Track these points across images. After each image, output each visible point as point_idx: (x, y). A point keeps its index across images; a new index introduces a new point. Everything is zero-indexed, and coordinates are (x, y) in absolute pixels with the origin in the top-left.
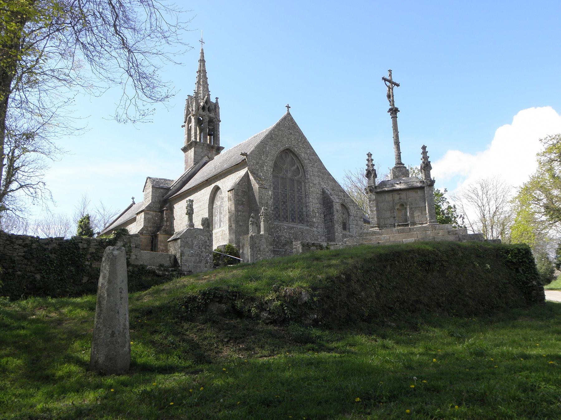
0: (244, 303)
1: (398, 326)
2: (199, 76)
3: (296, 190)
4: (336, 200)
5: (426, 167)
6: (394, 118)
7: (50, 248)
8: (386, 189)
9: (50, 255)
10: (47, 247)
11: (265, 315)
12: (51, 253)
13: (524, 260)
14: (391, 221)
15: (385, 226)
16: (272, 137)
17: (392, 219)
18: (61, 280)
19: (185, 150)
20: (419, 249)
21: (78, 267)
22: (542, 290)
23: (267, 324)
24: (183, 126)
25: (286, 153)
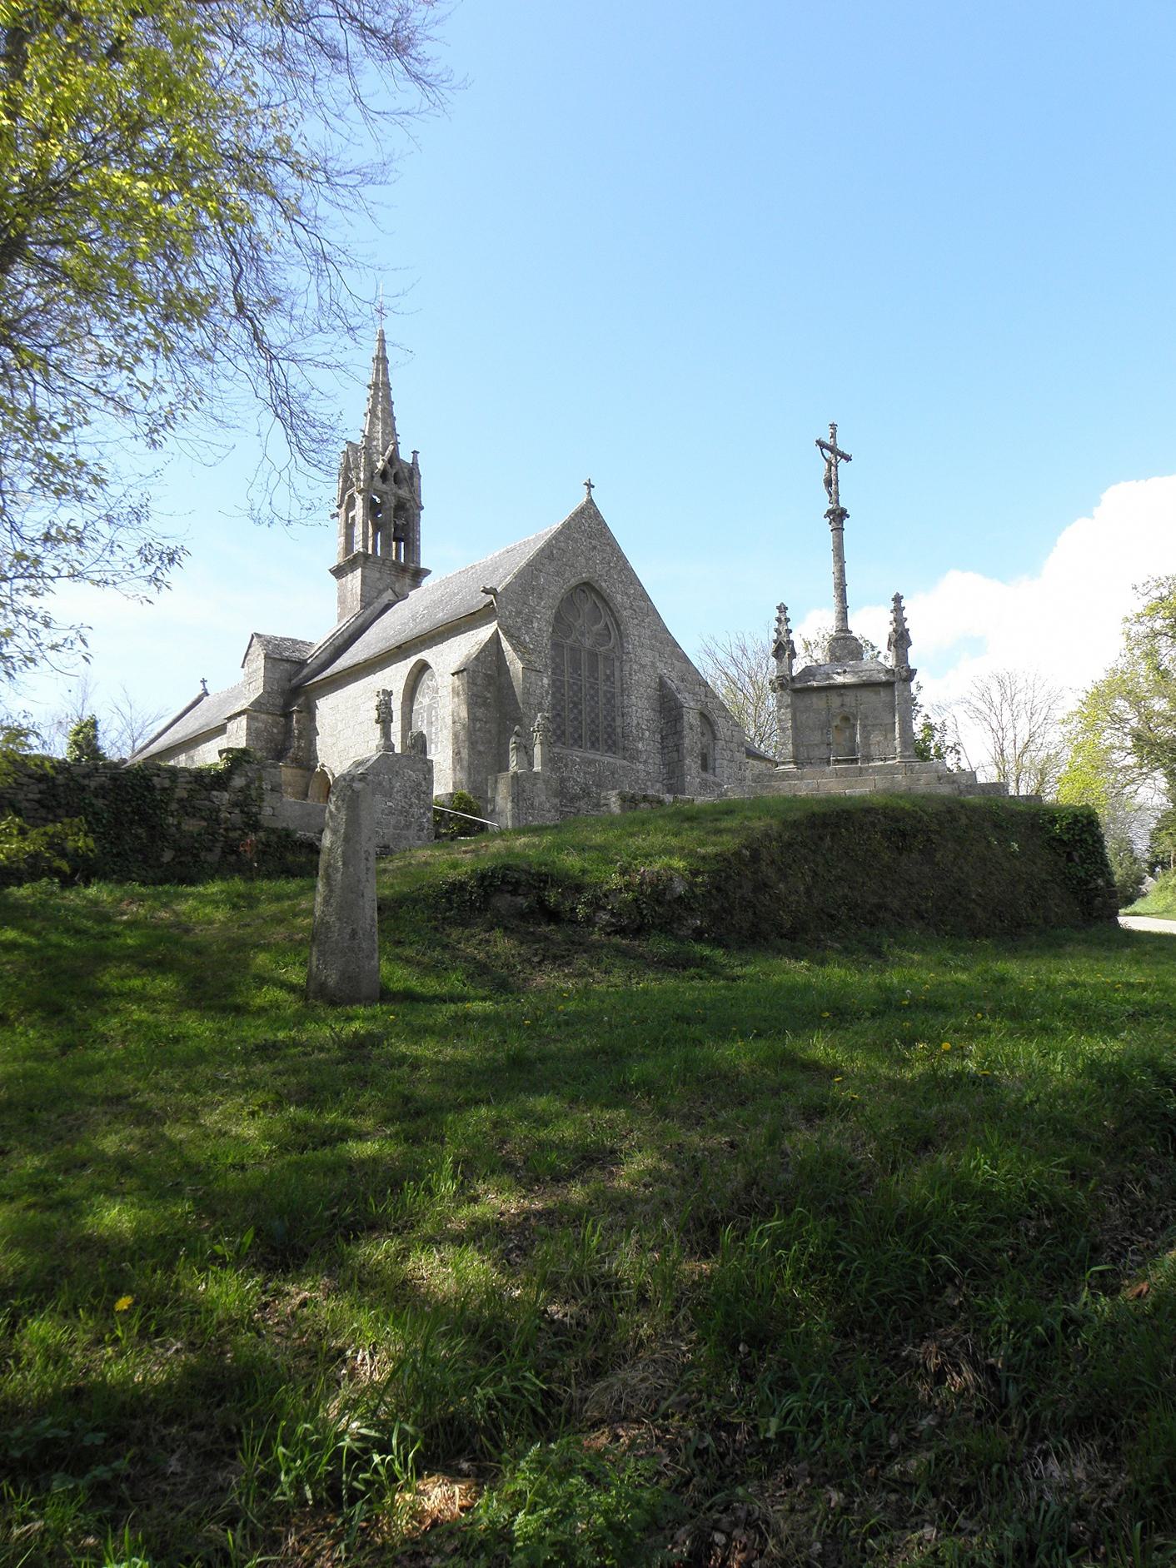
0: (562, 894)
1: (846, 948)
2: (374, 396)
3: (602, 677)
4: (688, 702)
5: (900, 640)
6: (838, 530)
7: (93, 784)
8: (815, 684)
9: (94, 801)
10: (86, 782)
11: (604, 917)
12: (96, 796)
13: (1084, 836)
14: (821, 752)
15: (809, 762)
16: (552, 553)
17: (823, 748)
18: (118, 855)
19: (339, 572)
20: (885, 807)
21: (153, 827)
22: (1117, 914)
23: (609, 934)
24: (333, 516)
25: (580, 593)
